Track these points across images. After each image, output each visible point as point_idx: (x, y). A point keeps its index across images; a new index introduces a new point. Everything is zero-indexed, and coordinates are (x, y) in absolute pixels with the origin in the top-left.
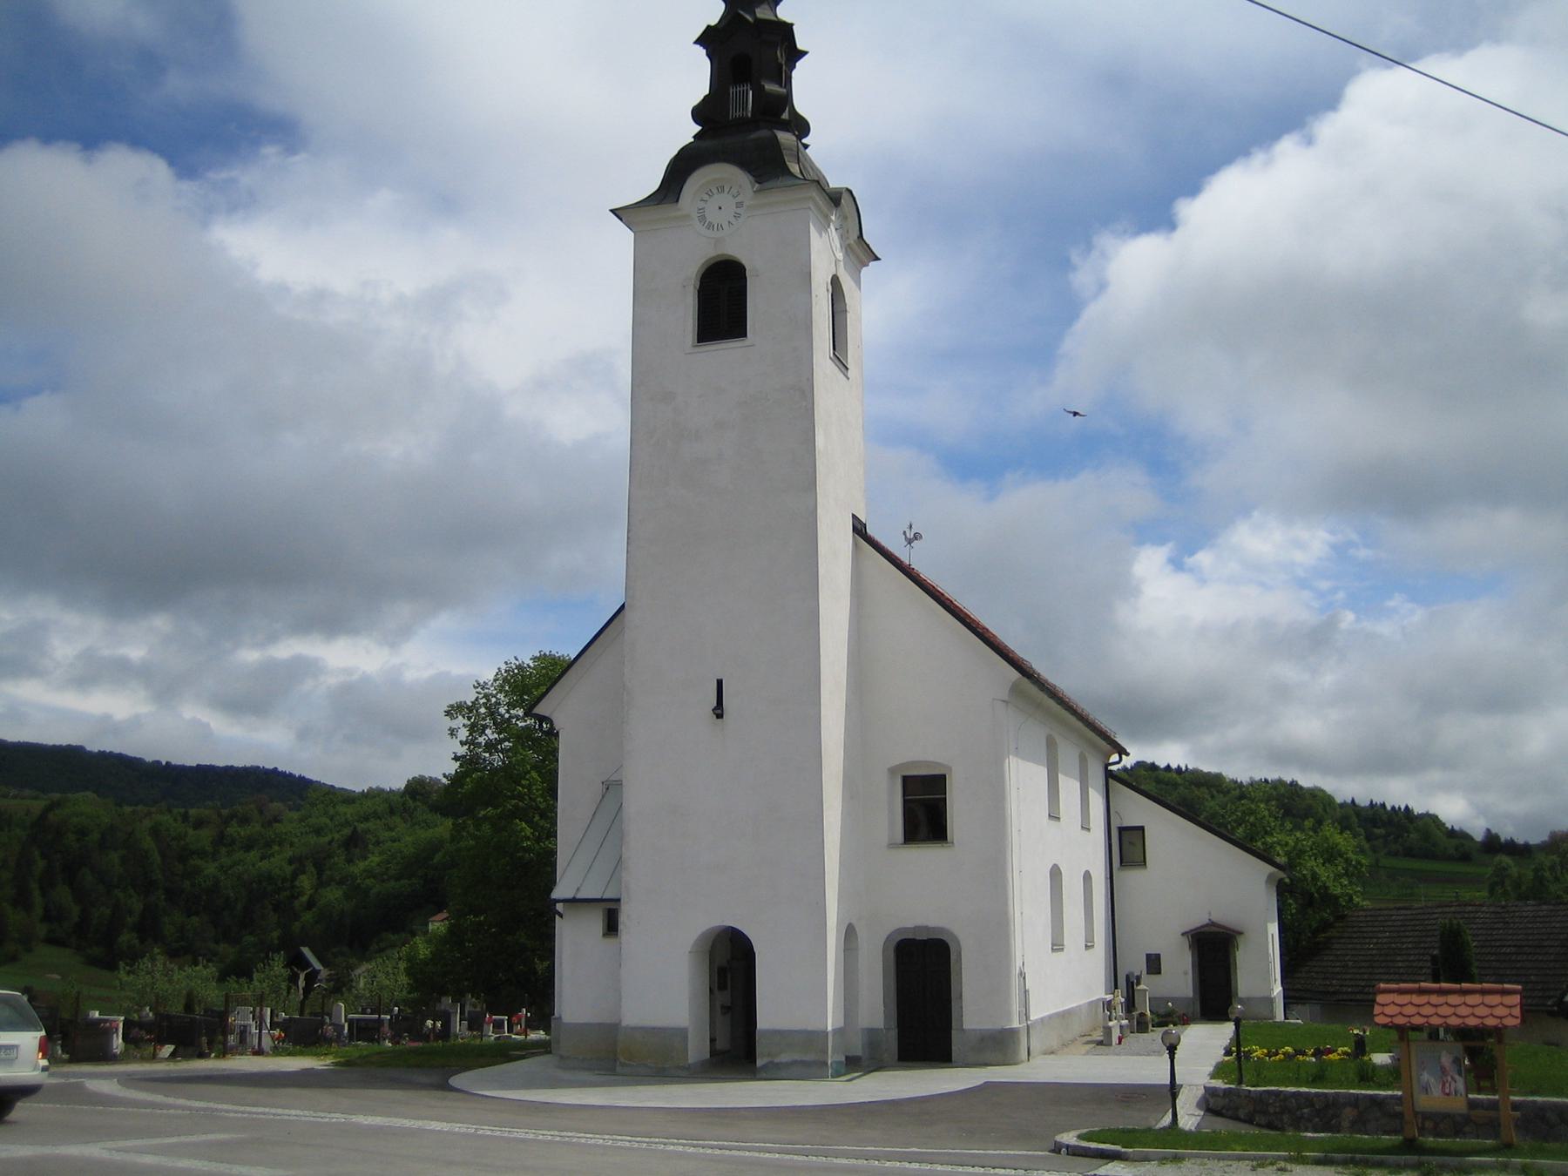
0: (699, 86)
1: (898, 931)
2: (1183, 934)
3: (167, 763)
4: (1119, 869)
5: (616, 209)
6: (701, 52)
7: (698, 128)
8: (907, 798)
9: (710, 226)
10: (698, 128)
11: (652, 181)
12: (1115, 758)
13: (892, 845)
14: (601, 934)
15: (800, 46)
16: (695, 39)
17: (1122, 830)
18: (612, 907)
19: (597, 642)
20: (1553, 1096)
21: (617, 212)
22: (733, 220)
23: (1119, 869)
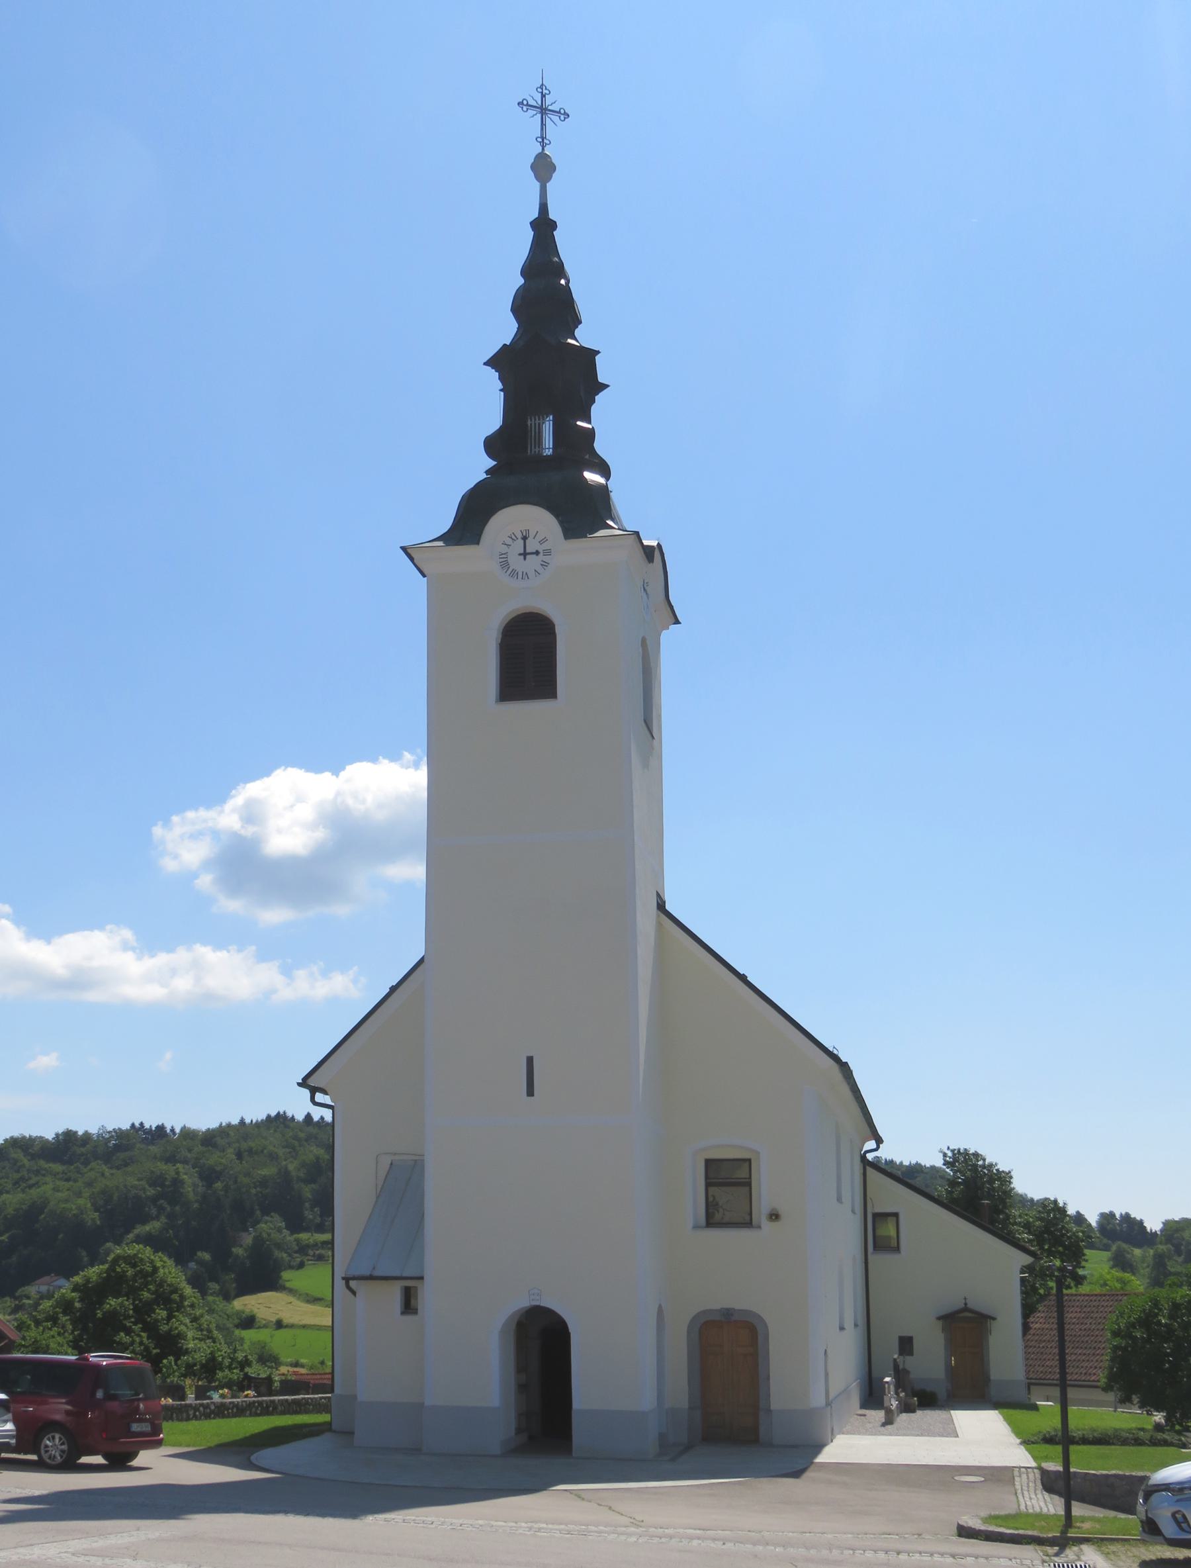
0: (492, 418)
1: (705, 1312)
2: (939, 1318)
3: (30, 1136)
4: (873, 1253)
5: (413, 546)
6: (493, 375)
7: (491, 463)
8: (708, 1181)
9: (514, 574)
10: (491, 463)
11: (445, 521)
12: (871, 1144)
13: (696, 1227)
14: (399, 1313)
15: (601, 379)
16: (485, 360)
17: (876, 1216)
18: (407, 1285)
19: (379, 1010)
20: (281, 1396)
21: (409, 551)
22: (540, 569)
23: (873, 1253)
